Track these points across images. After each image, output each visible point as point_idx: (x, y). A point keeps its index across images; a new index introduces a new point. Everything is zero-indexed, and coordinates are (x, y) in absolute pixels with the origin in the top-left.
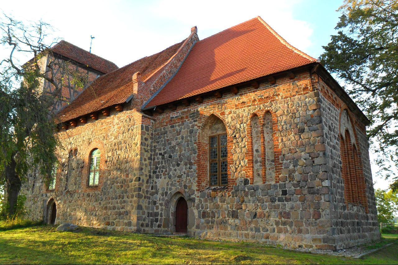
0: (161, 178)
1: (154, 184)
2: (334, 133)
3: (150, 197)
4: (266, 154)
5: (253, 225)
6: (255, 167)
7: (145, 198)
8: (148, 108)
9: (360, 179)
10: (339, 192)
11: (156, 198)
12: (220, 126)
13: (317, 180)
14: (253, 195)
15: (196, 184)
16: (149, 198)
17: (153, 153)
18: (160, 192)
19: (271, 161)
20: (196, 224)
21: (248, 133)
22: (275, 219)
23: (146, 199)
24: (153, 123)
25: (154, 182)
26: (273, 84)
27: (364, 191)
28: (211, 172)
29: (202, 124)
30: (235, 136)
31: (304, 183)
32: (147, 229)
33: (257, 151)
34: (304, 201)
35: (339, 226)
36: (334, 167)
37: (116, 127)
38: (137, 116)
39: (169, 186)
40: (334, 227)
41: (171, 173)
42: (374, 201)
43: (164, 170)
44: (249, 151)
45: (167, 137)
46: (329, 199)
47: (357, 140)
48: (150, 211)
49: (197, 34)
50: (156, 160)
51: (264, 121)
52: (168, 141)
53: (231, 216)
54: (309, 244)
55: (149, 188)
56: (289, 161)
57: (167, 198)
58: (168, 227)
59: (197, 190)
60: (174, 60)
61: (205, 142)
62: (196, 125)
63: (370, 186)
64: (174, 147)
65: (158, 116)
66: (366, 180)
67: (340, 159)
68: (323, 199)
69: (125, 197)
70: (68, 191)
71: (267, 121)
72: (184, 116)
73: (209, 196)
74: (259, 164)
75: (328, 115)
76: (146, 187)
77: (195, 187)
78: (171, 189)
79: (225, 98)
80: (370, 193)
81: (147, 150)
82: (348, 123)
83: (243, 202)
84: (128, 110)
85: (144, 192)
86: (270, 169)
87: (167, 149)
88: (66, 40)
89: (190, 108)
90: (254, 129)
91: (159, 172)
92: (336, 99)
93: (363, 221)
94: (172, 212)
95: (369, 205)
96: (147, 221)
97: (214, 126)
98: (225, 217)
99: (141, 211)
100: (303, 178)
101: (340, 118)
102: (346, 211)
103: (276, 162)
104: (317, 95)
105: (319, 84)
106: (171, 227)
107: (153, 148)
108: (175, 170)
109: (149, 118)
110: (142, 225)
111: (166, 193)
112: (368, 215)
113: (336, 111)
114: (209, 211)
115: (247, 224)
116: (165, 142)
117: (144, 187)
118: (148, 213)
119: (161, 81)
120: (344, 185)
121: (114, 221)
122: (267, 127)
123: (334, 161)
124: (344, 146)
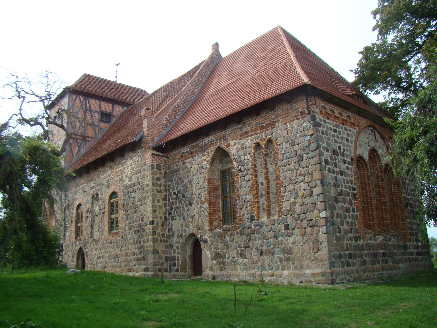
1: (170, 227)
4: (271, 186)
5: (260, 264)
7: (161, 241)
10: (348, 222)
11: (173, 241)
13: (316, 211)
16: (166, 242)
17: (168, 193)
18: (176, 234)
20: (209, 266)
21: (252, 165)
23: (162, 243)
24: (165, 161)
25: (170, 224)
30: (240, 169)
32: (165, 274)
34: (304, 235)
37: (130, 168)
38: (148, 156)
40: (333, 260)
41: (185, 214)
43: (178, 211)
44: (254, 185)
45: (180, 175)
46: (327, 230)
48: (168, 256)
50: (171, 201)
51: (266, 151)
54: (309, 279)
55: (165, 231)
57: (182, 241)
58: (185, 270)
59: (209, 230)
61: (215, 177)
62: (205, 160)
64: (186, 186)
70: (94, 239)
72: (194, 150)
74: (264, 198)
76: (162, 230)
77: (207, 228)
78: (185, 231)
83: (250, 240)
84: (139, 149)
85: (159, 236)
86: (274, 203)
88: (89, 73)
90: (258, 160)
91: (174, 213)
95: (410, 233)
96: (165, 266)
97: (224, 159)
99: (157, 256)
100: (302, 210)
101: (357, 138)
102: (361, 242)
103: (278, 195)
108: (188, 210)
109: (159, 156)
110: (160, 270)
111: (182, 235)
112: (408, 244)
113: (350, 130)
117: (159, 230)
118: (166, 257)
119: (175, 112)
120: (358, 213)
121: (134, 268)
122: (270, 157)
123: (341, 188)
124: (368, 169)
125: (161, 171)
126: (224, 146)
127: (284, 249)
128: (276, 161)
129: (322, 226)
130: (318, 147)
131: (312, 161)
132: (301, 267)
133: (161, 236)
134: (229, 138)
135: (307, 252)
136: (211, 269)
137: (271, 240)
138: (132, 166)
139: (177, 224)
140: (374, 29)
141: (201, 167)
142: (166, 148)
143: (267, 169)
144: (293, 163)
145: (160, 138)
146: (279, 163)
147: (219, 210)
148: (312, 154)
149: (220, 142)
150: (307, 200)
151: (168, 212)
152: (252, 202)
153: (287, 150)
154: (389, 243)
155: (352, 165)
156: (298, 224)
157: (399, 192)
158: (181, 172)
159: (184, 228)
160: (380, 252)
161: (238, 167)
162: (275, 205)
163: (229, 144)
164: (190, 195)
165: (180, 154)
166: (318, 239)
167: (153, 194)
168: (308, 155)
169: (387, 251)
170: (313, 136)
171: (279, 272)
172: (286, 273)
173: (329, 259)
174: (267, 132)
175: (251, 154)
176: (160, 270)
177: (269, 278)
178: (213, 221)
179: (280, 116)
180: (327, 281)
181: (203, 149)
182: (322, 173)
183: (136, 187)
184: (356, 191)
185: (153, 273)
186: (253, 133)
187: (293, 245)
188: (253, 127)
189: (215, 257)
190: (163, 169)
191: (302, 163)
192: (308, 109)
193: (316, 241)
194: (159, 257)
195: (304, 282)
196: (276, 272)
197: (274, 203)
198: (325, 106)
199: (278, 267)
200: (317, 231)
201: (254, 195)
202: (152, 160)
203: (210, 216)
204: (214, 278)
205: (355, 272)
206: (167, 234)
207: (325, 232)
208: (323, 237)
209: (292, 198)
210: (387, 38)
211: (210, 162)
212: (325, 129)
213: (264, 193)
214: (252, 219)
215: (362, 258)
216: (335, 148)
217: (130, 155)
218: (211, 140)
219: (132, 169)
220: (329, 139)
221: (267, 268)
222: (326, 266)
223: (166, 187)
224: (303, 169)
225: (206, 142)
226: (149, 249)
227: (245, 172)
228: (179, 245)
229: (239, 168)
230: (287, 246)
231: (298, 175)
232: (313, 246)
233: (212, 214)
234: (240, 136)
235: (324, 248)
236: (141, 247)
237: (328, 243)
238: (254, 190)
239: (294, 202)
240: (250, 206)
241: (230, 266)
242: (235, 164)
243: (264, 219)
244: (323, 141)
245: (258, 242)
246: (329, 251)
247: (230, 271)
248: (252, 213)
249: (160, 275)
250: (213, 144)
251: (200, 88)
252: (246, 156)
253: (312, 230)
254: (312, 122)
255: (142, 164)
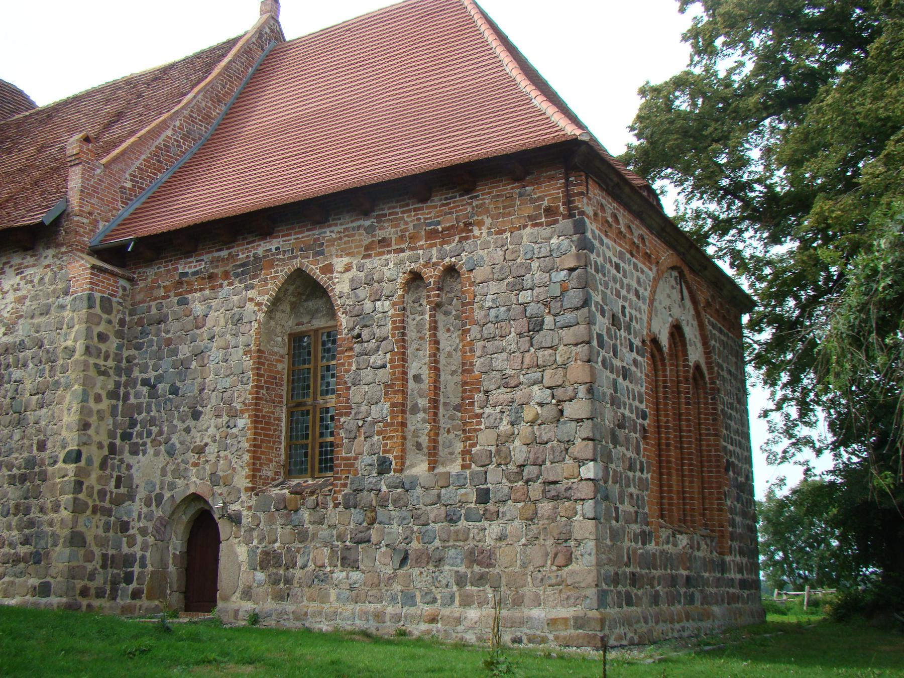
0: (144, 453)
2: (629, 334)
3: (110, 510)
4: (442, 387)
5: (397, 587)
6: (409, 425)
7: (95, 511)
8: (105, 245)
9: (710, 461)
10: (631, 495)
11: (129, 513)
12: (320, 303)
13: (569, 461)
14: (402, 503)
15: (244, 473)
16: (108, 512)
17: (124, 379)
18: (141, 494)
19: (454, 409)
20: (241, 586)
21: (394, 329)
22: (456, 568)
23: (98, 516)
24: (124, 289)
25: (124, 466)
26: (467, 192)
27: (719, 493)
28: (290, 438)
29: (266, 297)
30: (359, 336)
31: (534, 470)
32: (97, 603)
33: (417, 378)
34: (531, 520)
35: (624, 586)
36: (621, 426)
37: (11, 297)
38: (79, 270)
39: (169, 478)
40: (605, 587)
41: (174, 439)
42: (749, 522)
43: (155, 429)
44: (397, 379)
45: (168, 332)
46: (595, 512)
47: (710, 352)
48: (111, 552)
49: (278, 22)
50: (132, 400)
51: (438, 296)
52: (168, 345)
53: (339, 563)
54: (538, 633)
55: (107, 484)
56: (499, 409)
59: (247, 489)
60: (200, 96)
61: (276, 349)
62: (251, 300)
63: (741, 479)
64: (184, 364)
65: (140, 267)
66: (729, 465)
67: (643, 406)
68: (580, 513)
69: (33, 509)
71: (449, 295)
72: (219, 271)
73: (282, 506)
74: (421, 415)
75: (611, 284)
76: (99, 479)
77: (241, 481)
78: (172, 486)
79: (336, 225)
80: (738, 499)
81: (103, 369)
82: (682, 306)
83: (373, 523)
84: (48, 248)
85: (90, 495)
87: (164, 367)
89: (235, 249)
90: (412, 317)
91: (140, 435)
92: (643, 239)
93: (706, 575)
94: (174, 554)
95: (731, 533)
96: (99, 581)
97: (306, 304)
98: (323, 566)
99: (82, 551)
100: (532, 456)
101: (653, 293)
102: (651, 547)
103: (466, 411)
104: (579, 228)
105: (590, 199)
106: (175, 598)
107: (124, 364)
108: (188, 430)
109: (112, 274)
110: (84, 592)
111: (159, 497)
112: (728, 558)
113: (642, 272)
114: (279, 548)
115: (382, 585)
116: (160, 348)
117: (92, 480)
118: (104, 556)
119: (158, 161)
120: (649, 476)
122: (447, 313)
123: (622, 410)
125: (112, 317)
126: (314, 269)
127: (471, 552)
128: (464, 325)
129: (584, 500)
130: (586, 303)
131: (568, 335)
132: (518, 602)
133: (95, 496)
134: (333, 249)
135: (538, 562)
136: (247, 594)
137: (437, 526)
138: (20, 294)
139: (146, 467)
140: (685, 38)
141: (237, 317)
142: (122, 257)
143: (437, 342)
144: (513, 334)
145: (113, 227)
146: (475, 331)
147: (279, 437)
148: (569, 317)
149: (303, 258)
150: (546, 432)
151: (119, 431)
152: (387, 425)
153: (500, 300)
154: (697, 553)
155: (643, 356)
156: (518, 490)
157: (715, 435)
158: (174, 326)
159: (169, 478)
160: (682, 575)
161: (353, 329)
162: (451, 436)
163: (331, 265)
164: (196, 391)
165: (172, 276)
166: (570, 532)
167: (86, 378)
168: (557, 319)
169: (693, 574)
170: (575, 273)
171: (456, 610)
172: (473, 614)
173: (597, 585)
174: (447, 247)
175: (395, 299)
176: (84, 592)
177: (424, 627)
178: (261, 464)
179: (487, 211)
180: (589, 641)
181: (249, 270)
182: (591, 367)
183: (29, 353)
184: (647, 421)
185: (64, 600)
186: (404, 246)
187: (498, 544)
188: (406, 230)
189: (261, 562)
190: (118, 311)
191: (538, 337)
192: (568, 202)
193: (563, 536)
194: (85, 556)
195: (525, 640)
196: (446, 611)
197: (448, 432)
198: (604, 202)
199: (452, 597)
200: (570, 513)
201: (393, 405)
202: (91, 283)
203: (254, 452)
204: (255, 619)
205: (642, 620)
206: (111, 493)
207: (591, 516)
208: (583, 527)
209: (505, 422)
210: (715, 63)
211: (268, 307)
212: (601, 259)
213: (423, 402)
214: (383, 467)
215: (652, 587)
216: (615, 309)
217: (16, 260)
218: (277, 248)
219: (21, 300)
220: (606, 286)
221: (418, 600)
222: (588, 601)
223: (120, 361)
224: (540, 353)
225: (260, 251)
226: (58, 532)
227: (373, 344)
228: (150, 526)
229: (356, 331)
230: (480, 544)
231: (525, 366)
232: (554, 550)
233: (260, 446)
234: (366, 250)
235: (586, 556)
236: (31, 524)
237: (597, 545)
238: (395, 392)
239: (509, 432)
240: (379, 433)
241: (306, 589)
242: (344, 320)
243: (419, 468)
244: (596, 289)
245: (397, 529)
246: (599, 564)
247: (305, 602)
248: (385, 451)
249: (84, 607)
250: (280, 260)
251: (224, 108)
252: (379, 303)
253: (555, 508)
254: (575, 238)
255: (54, 291)
